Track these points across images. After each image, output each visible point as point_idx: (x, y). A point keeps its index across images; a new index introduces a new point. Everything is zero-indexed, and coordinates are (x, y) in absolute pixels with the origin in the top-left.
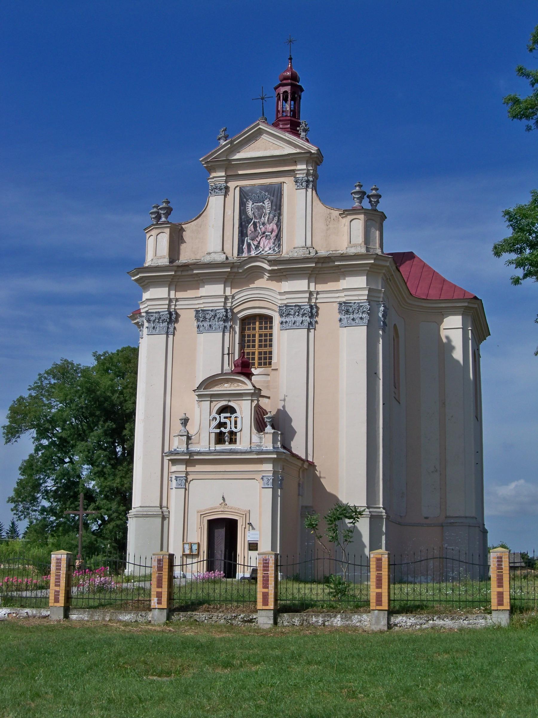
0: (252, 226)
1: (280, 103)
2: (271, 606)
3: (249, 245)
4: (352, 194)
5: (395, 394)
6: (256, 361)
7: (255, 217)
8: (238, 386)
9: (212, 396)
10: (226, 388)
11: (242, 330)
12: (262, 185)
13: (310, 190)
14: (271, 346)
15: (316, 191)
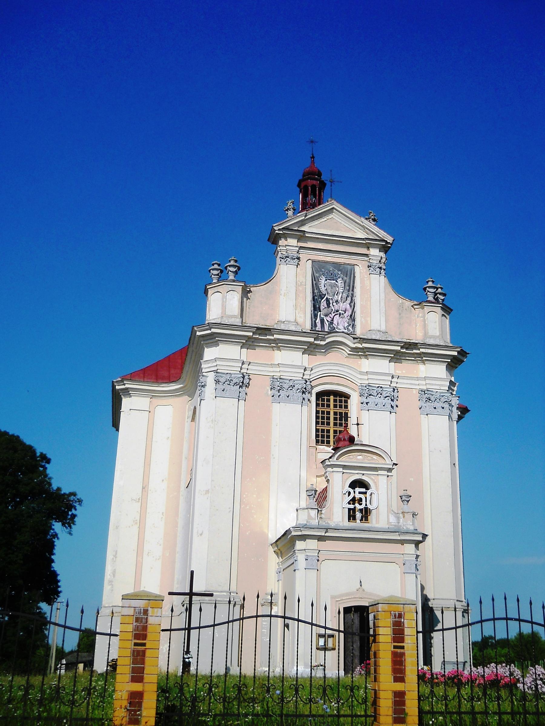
3: (322, 321)
9: (344, 467)
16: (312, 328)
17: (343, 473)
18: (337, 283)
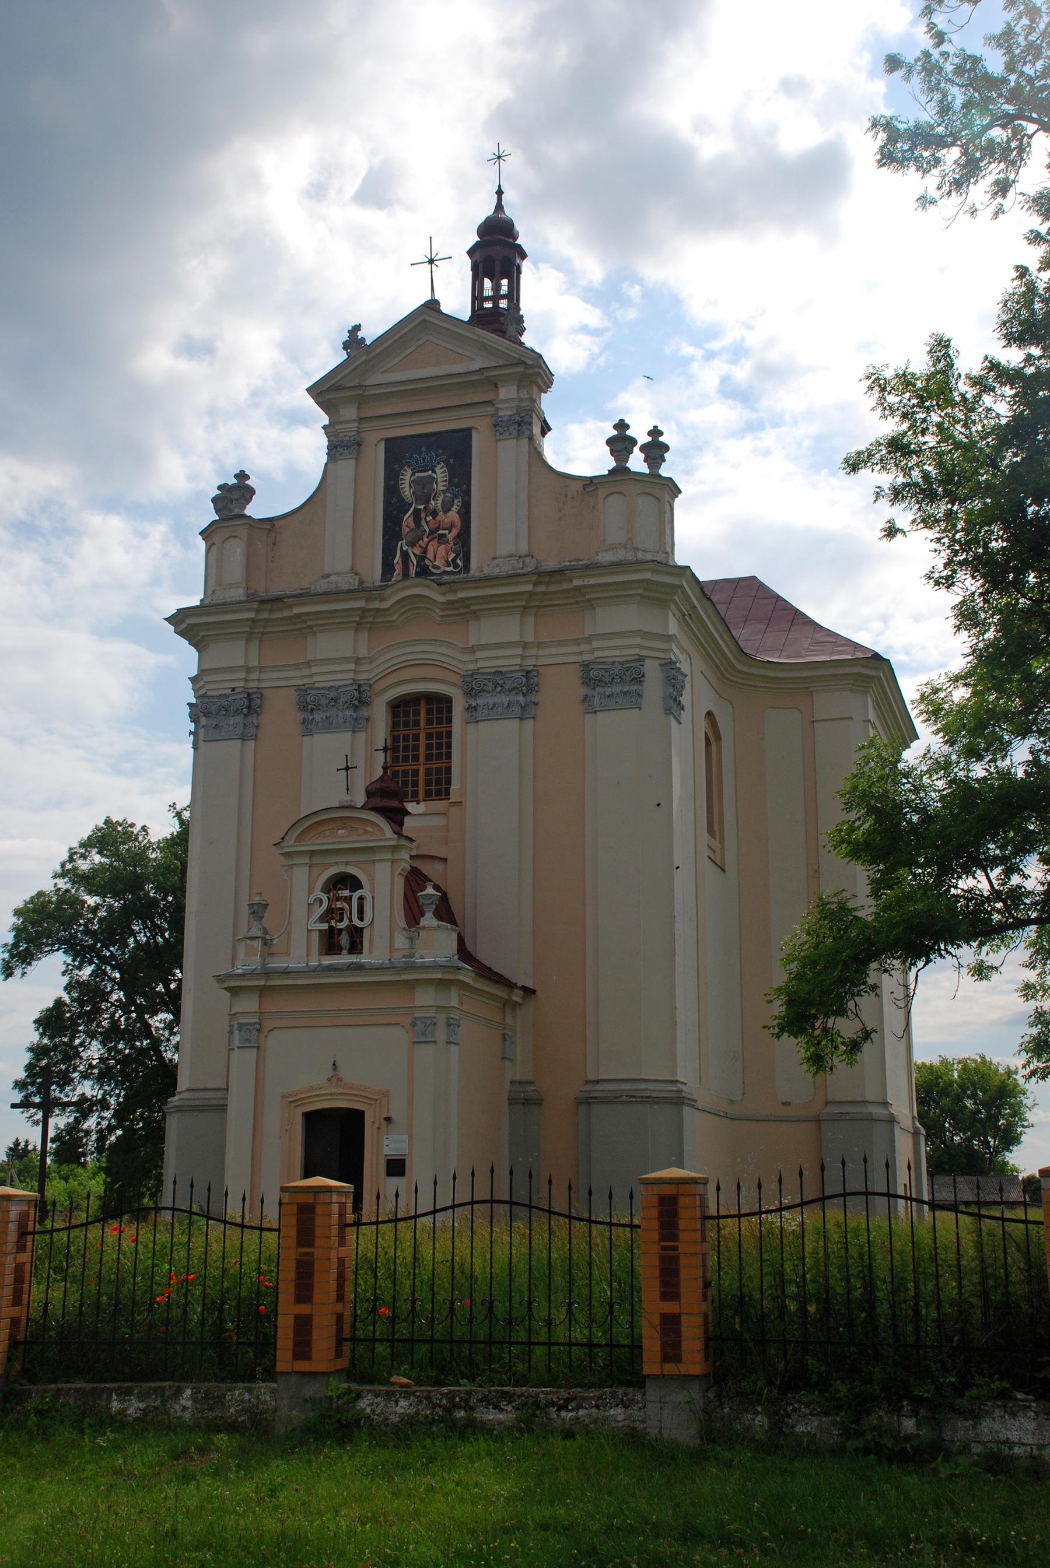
0: (412, 518)
3: (405, 556)
5: (714, 852)
8: (366, 832)
9: (312, 853)
10: (342, 838)
14: (449, 756)
17: (311, 866)
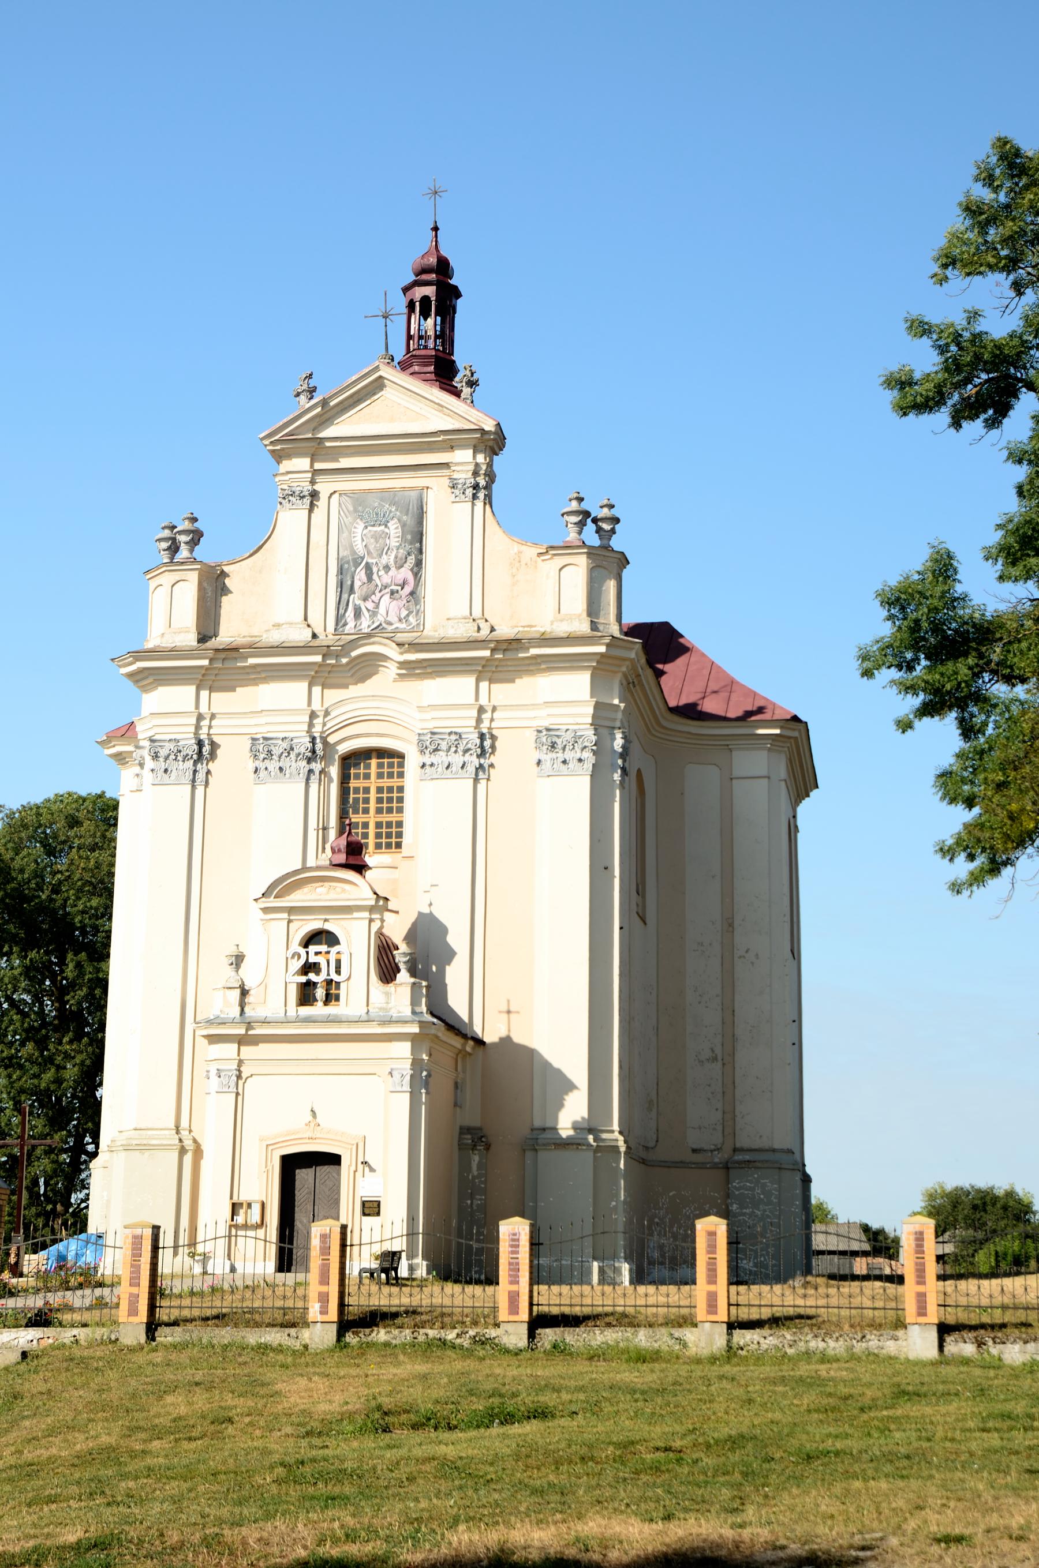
0: (364, 571)
1: (414, 319)
2: (524, 1316)
4: (563, 515)
6: (371, 841)
7: (369, 553)
8: (344, 890)
9: (291, 910)
11: (345, 779)
12: (383, 490)
13: (479, 504)
14: (400, 810)
15: (491, 507)
16: (335, 630)
18: (387, 530)
